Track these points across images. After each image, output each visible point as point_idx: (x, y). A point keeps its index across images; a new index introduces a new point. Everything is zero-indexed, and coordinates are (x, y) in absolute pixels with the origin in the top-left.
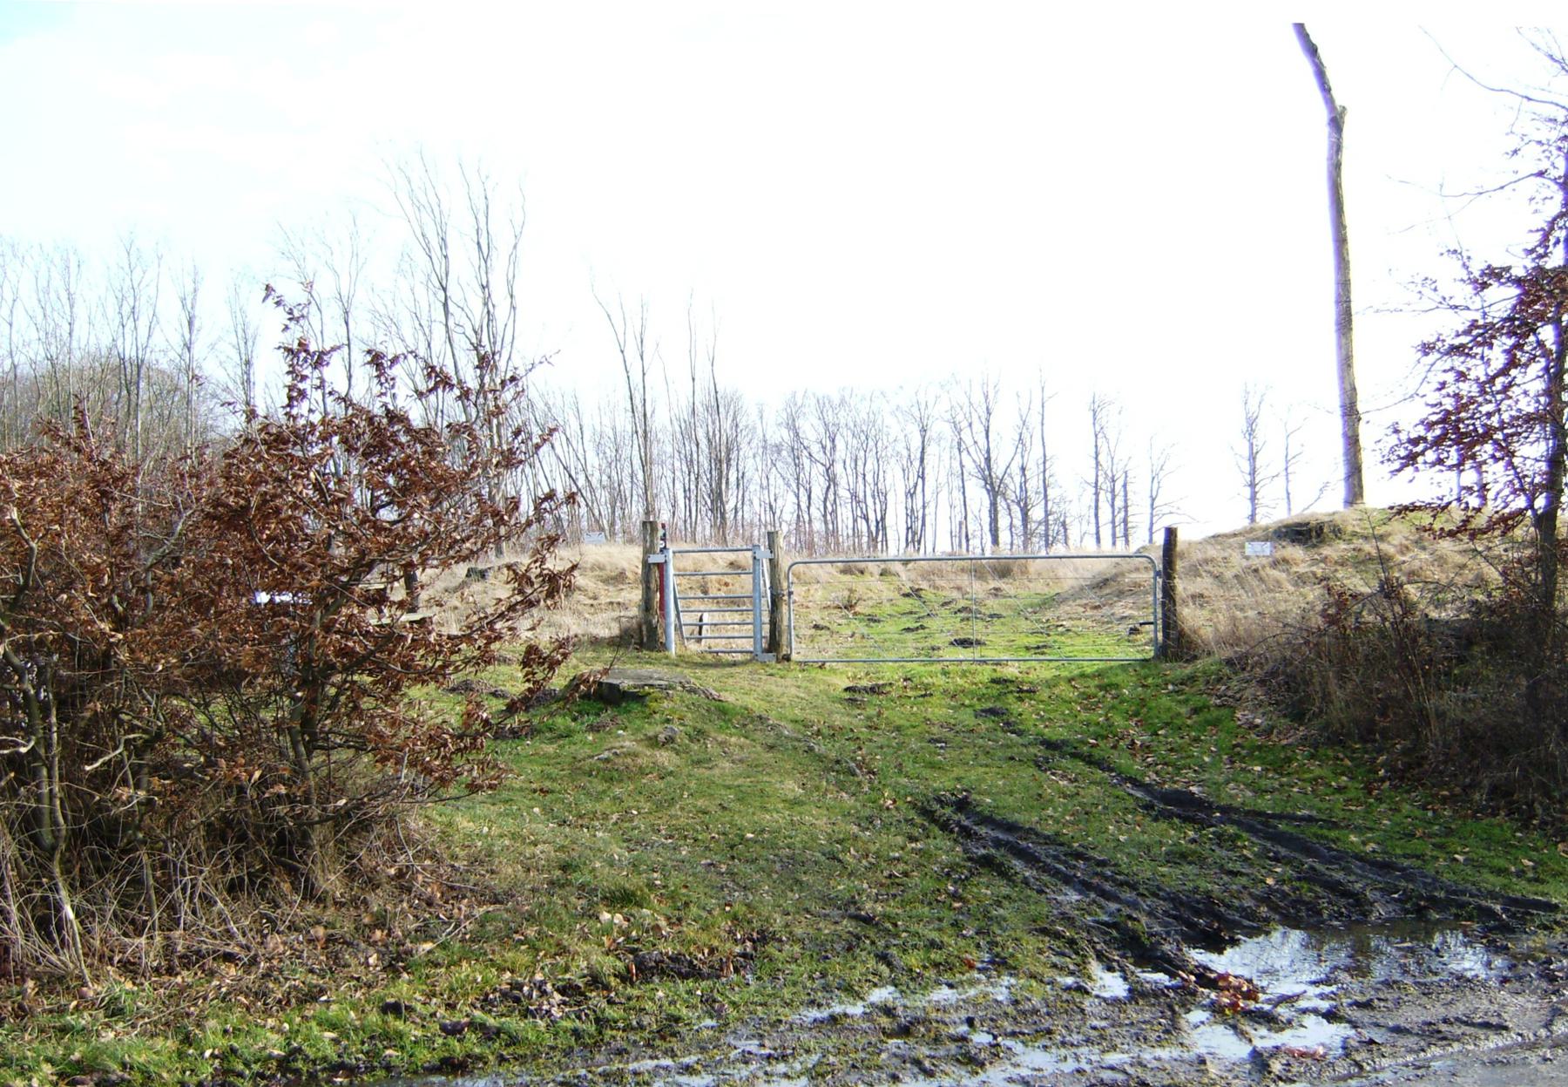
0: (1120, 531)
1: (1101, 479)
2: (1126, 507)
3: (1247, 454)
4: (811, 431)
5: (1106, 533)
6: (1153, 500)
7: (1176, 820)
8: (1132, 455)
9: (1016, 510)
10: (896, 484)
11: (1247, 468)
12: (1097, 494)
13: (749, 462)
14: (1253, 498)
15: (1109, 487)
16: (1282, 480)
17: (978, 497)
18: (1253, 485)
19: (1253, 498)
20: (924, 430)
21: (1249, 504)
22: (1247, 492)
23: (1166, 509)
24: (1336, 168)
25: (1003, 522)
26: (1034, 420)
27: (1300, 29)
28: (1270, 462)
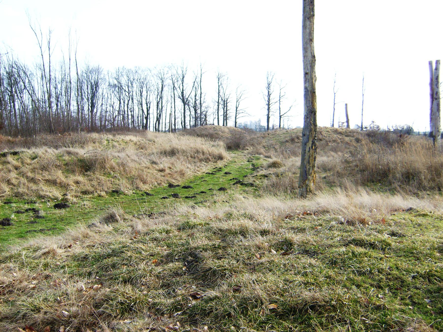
1: (220, 101)
4: (124, 81)
6: (237, 108)
12: (218, 106)
13: (103, 89)
14: (269, 109)
18: (269, 105)
19: (269, 109)
23: (241, 111)
25: (187, 113)
27: (346, 105)
28: (274, 97)
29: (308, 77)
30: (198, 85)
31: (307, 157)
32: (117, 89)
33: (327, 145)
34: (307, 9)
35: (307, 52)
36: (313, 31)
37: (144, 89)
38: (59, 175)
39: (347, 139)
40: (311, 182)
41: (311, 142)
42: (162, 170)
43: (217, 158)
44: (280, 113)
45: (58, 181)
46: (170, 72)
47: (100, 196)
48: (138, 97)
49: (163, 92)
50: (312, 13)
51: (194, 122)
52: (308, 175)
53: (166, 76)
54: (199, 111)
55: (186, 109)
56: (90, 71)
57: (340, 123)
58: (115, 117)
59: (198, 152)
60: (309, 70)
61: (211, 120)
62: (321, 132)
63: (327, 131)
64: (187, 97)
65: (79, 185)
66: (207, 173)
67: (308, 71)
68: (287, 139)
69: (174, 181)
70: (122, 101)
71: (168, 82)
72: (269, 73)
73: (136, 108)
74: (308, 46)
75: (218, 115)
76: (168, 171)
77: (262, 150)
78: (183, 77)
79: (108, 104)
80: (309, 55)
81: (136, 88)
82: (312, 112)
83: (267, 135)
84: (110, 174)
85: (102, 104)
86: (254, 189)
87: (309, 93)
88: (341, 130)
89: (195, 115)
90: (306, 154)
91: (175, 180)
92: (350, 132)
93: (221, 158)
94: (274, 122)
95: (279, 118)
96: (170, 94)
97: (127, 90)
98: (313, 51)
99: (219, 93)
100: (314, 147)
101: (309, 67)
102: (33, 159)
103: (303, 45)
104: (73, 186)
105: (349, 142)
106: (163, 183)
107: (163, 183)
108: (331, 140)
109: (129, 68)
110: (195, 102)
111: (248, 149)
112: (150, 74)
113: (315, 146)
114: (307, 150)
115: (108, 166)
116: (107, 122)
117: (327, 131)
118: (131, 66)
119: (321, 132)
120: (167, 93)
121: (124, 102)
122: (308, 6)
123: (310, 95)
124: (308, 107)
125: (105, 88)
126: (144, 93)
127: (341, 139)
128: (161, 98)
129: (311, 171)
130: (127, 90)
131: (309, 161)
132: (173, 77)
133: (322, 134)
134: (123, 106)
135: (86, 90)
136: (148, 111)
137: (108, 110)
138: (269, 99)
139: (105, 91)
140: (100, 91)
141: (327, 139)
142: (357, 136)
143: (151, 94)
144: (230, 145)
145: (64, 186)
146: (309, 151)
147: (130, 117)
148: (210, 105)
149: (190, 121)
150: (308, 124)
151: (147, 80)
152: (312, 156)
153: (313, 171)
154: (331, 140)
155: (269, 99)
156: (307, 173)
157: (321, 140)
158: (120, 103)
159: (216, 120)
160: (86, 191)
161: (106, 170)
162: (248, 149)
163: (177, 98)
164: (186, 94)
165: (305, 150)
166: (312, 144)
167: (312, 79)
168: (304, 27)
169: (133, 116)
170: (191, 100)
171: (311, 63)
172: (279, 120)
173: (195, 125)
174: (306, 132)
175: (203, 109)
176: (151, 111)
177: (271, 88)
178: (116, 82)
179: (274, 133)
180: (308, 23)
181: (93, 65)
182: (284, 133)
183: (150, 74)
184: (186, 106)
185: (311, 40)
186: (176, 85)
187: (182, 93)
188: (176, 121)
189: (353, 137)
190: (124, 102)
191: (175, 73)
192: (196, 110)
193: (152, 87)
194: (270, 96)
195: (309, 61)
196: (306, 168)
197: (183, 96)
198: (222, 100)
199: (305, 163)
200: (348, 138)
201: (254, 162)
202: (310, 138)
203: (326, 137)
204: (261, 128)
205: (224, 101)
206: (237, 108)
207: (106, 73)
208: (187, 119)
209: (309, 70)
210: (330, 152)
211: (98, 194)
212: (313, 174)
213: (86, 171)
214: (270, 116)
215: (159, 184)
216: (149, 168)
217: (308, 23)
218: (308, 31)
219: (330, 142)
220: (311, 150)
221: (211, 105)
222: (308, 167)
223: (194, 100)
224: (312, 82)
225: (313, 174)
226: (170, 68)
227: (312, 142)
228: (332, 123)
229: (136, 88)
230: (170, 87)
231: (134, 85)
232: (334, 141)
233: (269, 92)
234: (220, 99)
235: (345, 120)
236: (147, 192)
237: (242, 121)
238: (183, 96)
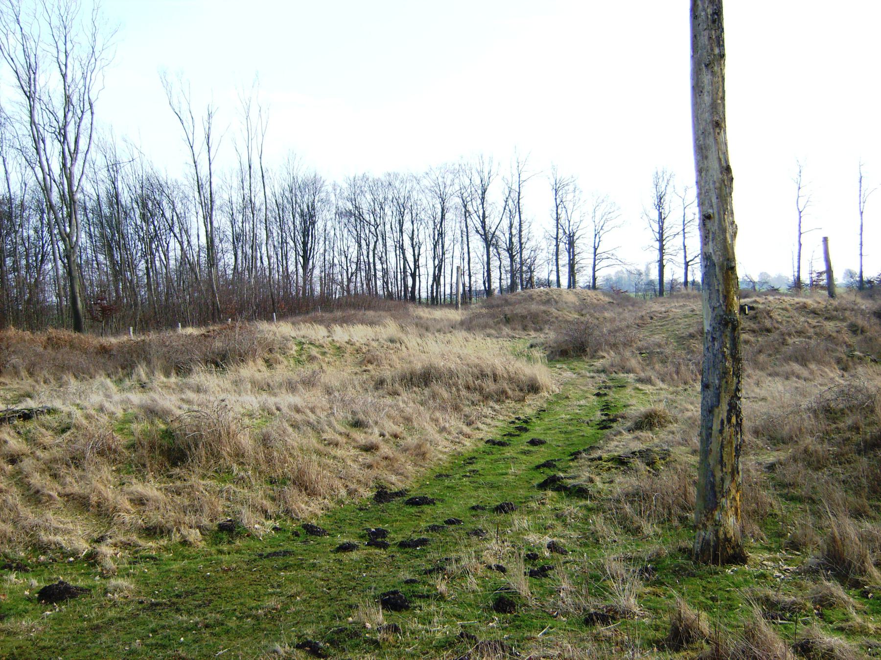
1: (560, 236)
3: (657, 219)
4: (365, 203)
6: (596, 249)
7: (614, 389)
9: (505, 255)
10: (425, 236)
11: (657, 229)
12: (557, 246)
13: (325, 221)
14: (661, 249)
16: (681, 237)
17: (477, 244)
18: (661, 240)
19: (661, 249)
20: (443, 201)
21: (657, 253)
22: (657, 245)
23: (605, 256)
25: (495, 263)
27: (825, 240)
29: (713, 226)
30: (514, 205)
31: (715, 446)
32: (353, 219)
33: (784, 343)
34: (704, 40)
35: (706, 158)
36: (723, 98)
37: (407, 218)
38: (102, 482)
39: (830, 326)
40: (730, 513)
41: (724, 407)
42: (369, 448)
43: (526, 388)
44: (685, 257)
45: (94, 499)
46: (457, 181)
47: (185, 543)
48: (395, 234)
49: (445, 223)
50: (717, 51)
52: (719, 495)
53: (449, 190)
55: (491, 254)
56: (295, 189)
57: (814, 275)
58: (352, 275)
59: (483, 375)
60: (715, 206)
61: (543, 272)
62: (768, 313)
63: (783, 309)
64: (493, 229)
65: (142, 508)
66: (488, 442)
67: (710, 211)
68: (691, 330)
69: (393, 478)
70: (363, 242)
71: (454, 201)
72: (660, 174)
73: (392, 256)
74: (710, 141)
75: (557, 265)
76: (385, 450)
77: (633, 363)
78: (484, 193)
79: (337, 249)
80: (714, 165)
81: (390, 214)
82: (726, 325)
83: (649, 321)
84: (229, 471)
85: (325, 251)
86: (586, 506)
87: (717, 269)
88: (816, 305)
89: (512, 265)
90: (713, 439)
91: (397, 474)
92: (836, 309)
93: (534, 388)
95: (683, 266)
96: (458, 225)
97: (373, 222)
98: (725, 153)
99: (557, 220)
100: (734, 420)
101: (714, 200)
102: (64, 431)
103: (696, 139)
104: (128, 512)
105: (834, 334)
106: (361, 490)
107: (361, 490)
108: (793, 330)
109: (376, 177)
110: (511, 239)
111: (603, 357)
112: (418, 187)
113: (737, 417)
114: (716, 427)
115: (226, 450)
117: (783, 309)
118: (377, 172)
119: (768, 313)
120: (453, 225)
121: (368, 245)
122: (706, 33)
123: (720, 277)
124: (714, 309)
125: (328, 217)
126: (407, 225)
127: (814, 327)
128: (441, 234)
129: (727, 483)
130: (373, 222)
131: (722, 457)
132: (463, 191)
133: (771, 317)
134: (365, 253)
135: (294, 222)
136: (416, 261)
137: (336, 261)
138: (661, 228)
139: (329, 224)
140: (319, 225)
141: (783, 328)
142: (853, 319)
143: (421, 228)
144: (564, 347)
145: (103, 513)
146: (721, 432)
147: (379, 274)
149: (500, 279)
150: (715, 355)
151: (412, 200)
152: (730, 442)
153: (734, 485)
154: (793, 330)
155: (661, 228)
156: (717, 489)
157: (768, 331)
158: (360, 246)
159: (555, 273)
160: (155, 528)
161: (222, 461)
162: (603, 357)
163: (472, 232)
164: (492, 222)
165: (711, 428)
166: (729, 412)
167: (724, 231)
168: (697, 89)
169: (385, 272)
170: (501, 235)
171: (720, 188)
172: (684, 271)
173: (512, 287)
174: (711, 380)
175: (526, 254)
176: (422, 261)
177: (666, 206)
178: (350, 206)
179: (664, 315)
180: (706, 78)
181: (303, 173)
182: (686, 316)
183: (418, 187)
184: (491, 249)
185: (718, 125)
186: (470, 208)
187: (483, 222)
188: (473, 279)
189: (844, 320)
190: (368, 245)
191: (467, 182)
192: (512, 257)
193: (423, 212)
194: (663, 223)
195: (714, 182)
196: (713, 476)
198: (565, 233)
199: (712, 462)
200: (832, 324)
201: (612, 396)
202: (723, 394)
203: (781, 323)
204: (650, 283)
205: (570, 236)
206: (596, 249)
207: (330, 189)
208: (495, 274)
209: (715, 206)
210: (791, 363)
211: (183, 536)
212: (733, 492)
213: (174, 465)
214: (665, 262)
215: (350, 493)
216: (337, 445)
217: (706, 78)
218: (707, 99)
219: (789, 335)
220: (726, 429)
221: (544, 244)
222: (719, 475)
223: (507, 236)
224: (725, 240)
225: (733, 492)
226: (456, 173)
227: (730, 404)
228: (796, 274)
229: (390, 214)
230: (458, 213)
231: (388, 211)
232: (800, 333)
233: (660, 213)
234: (561, 231)
235: (823, 268)
236: (314, 522)
237: (606, 272)
238: (484, 227)
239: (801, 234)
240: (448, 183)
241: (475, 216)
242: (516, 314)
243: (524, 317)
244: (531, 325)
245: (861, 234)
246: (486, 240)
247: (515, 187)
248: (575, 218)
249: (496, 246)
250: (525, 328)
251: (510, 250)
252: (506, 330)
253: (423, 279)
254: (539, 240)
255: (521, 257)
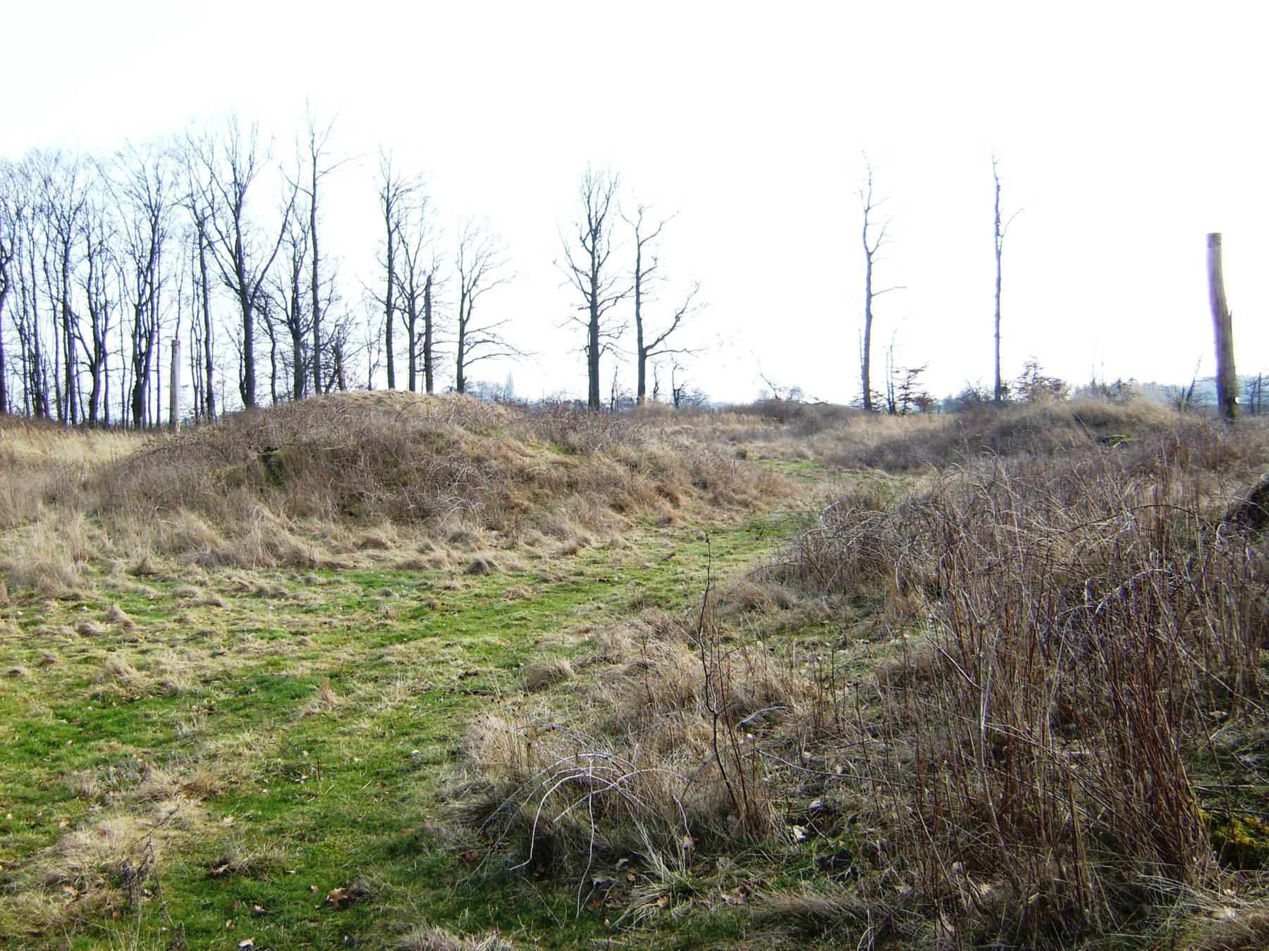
0: (420, 362)
2: (428, 333)
5: (401, 365)
6: (463, 323)
8: (436, 254)
9: (282, 330)
15: (407, 302)
17: (226, 306)
18: (594, 307)
24: (869, 274)
25: (261, 346)
26: (304, 201)
27: (1214, 240)
28: (617, 274)
30: (305, 234)
37: (78, 250)
44: (640, 340)
51: (292, 381)
53: (168, 197)
54: (309, 338)
61: (363, 371)
71: (179, 221)
89: (297, 354)
94: (618, 377)
95: (636, 359)
110: (295, 301)
116: (965, 633)
120: (176, 261)
148: (353, 299)
149: (273, 377)
175: (327, 327)
188: (216, 376)
192: (297, 335)
197: (240, 271)
206: (463, 323)
208: (262, 369)
221: (361, 315)
223: (289, 294)
234: (395, 289)
238: (240, 271)
239: (870, 296)
240: (167, 179)
241: (220, 246)
242: (311, 445)
243: (341, 460)
244: (376, 495)
245: (998, 297)
246: (242, 292)
247: (307, 183)
248: (424, 263)
249: (265, 312)
250: (350, 510)
251: (293, 322)
252: (267, 520)
253: (115, 378)
254: (351, 306)
255: (317, 338)
